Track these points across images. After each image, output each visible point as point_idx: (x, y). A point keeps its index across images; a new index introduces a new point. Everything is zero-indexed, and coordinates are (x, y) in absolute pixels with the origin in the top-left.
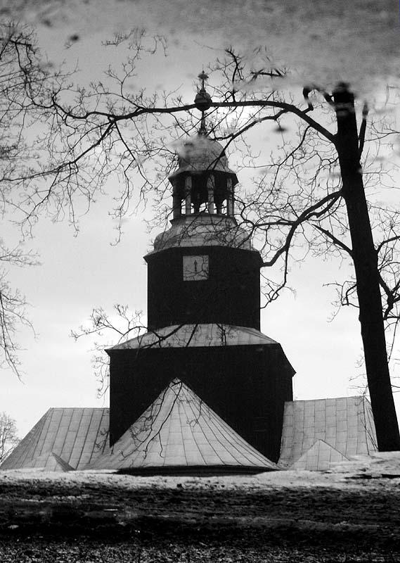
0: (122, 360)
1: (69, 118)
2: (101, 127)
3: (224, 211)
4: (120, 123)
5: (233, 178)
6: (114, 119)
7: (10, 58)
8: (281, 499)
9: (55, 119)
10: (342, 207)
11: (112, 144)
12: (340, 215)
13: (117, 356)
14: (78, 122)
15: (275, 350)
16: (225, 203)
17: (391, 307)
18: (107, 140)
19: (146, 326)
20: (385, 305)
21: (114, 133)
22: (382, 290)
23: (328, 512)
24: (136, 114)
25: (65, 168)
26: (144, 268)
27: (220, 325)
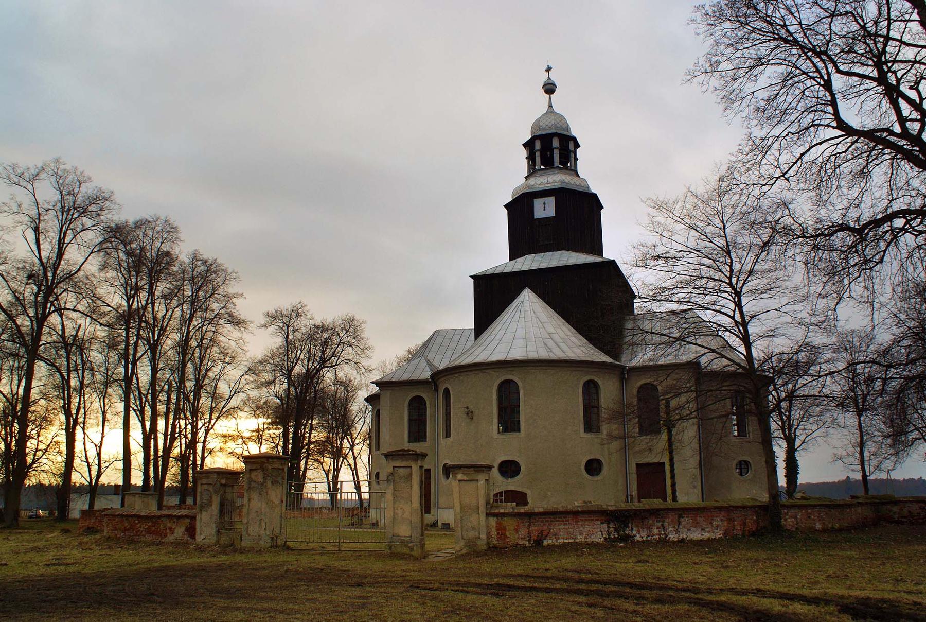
13: (603, 208)
15: (612, 263)
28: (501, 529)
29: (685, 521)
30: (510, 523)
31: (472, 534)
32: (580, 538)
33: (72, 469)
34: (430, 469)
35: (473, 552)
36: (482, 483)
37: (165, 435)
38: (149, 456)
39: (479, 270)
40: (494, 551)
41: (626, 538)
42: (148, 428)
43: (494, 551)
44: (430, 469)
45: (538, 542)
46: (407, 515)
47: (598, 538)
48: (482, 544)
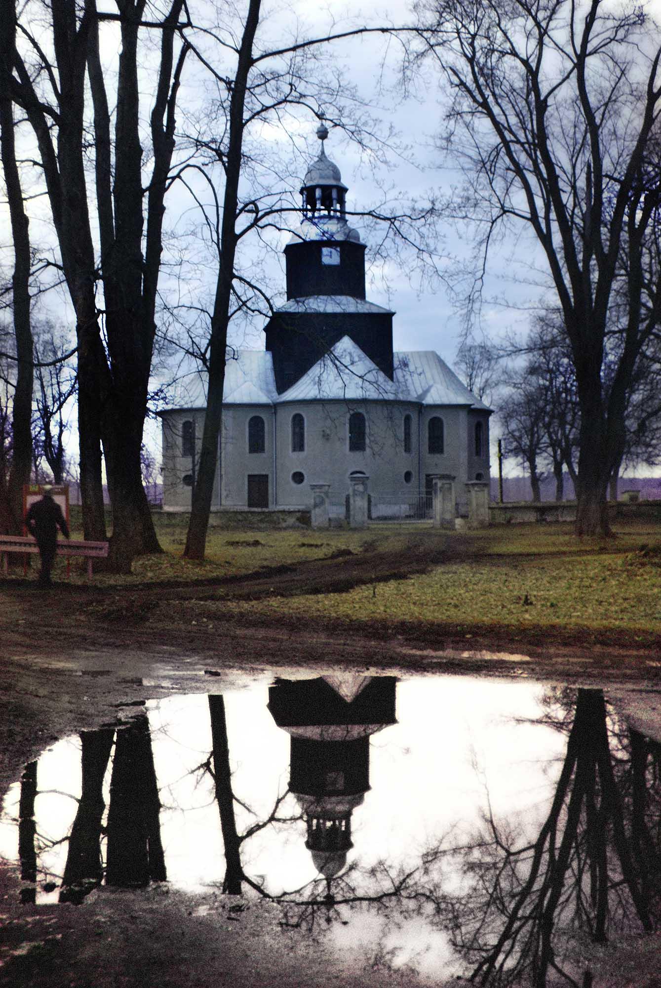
0: (387, 717)
1: (428, 894)
2: (407, 888)
3: (315, 821)
4: (392, 891)
5: (309, 845)
6: (397, 892)
7: (468, 936)
8: (303, 658)
9: (439, 893)
10: (241, 830)
11: (399, 876)
12: (242, 822)
13: (390, 719)
14: (421, 891)
15: (281, 721)
16: (314, 828)
17: (209, 759)
18: (402, 878)
19: (26, 116)
20: (212, 760)
21: (397, 883)
22: (214, 771)
23: (272, 645)
24: (382, 897)
25: (432, 856)
26: (373, 780)
27: (77, 386)
28: (493, 514)
29: (565, 512)
30: (497, 512)
31: (481, 518)
32: (526, 519)
33: (606, 733)
34: (267, 476)
35: (482, 526)
36: (486, 492)
37: (102, 142)
38: (567, 294)
39: (396, 725)
40: (491, 525)
41: (545, 520)
42: (548, 839)
43: (491, 525)
44: (267, 476)
45: (509, 522)
46: (449, 508)
47: (533, 519)
48: (487, 522)
